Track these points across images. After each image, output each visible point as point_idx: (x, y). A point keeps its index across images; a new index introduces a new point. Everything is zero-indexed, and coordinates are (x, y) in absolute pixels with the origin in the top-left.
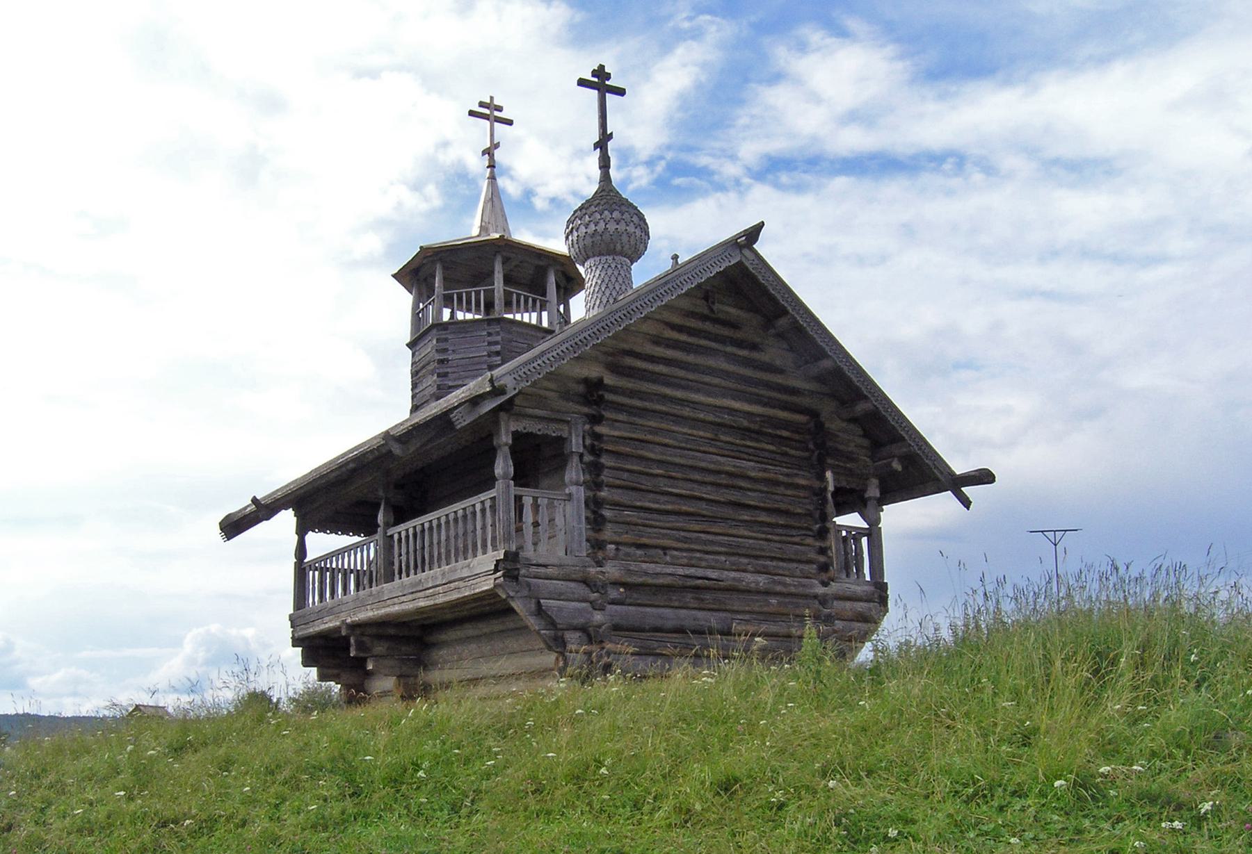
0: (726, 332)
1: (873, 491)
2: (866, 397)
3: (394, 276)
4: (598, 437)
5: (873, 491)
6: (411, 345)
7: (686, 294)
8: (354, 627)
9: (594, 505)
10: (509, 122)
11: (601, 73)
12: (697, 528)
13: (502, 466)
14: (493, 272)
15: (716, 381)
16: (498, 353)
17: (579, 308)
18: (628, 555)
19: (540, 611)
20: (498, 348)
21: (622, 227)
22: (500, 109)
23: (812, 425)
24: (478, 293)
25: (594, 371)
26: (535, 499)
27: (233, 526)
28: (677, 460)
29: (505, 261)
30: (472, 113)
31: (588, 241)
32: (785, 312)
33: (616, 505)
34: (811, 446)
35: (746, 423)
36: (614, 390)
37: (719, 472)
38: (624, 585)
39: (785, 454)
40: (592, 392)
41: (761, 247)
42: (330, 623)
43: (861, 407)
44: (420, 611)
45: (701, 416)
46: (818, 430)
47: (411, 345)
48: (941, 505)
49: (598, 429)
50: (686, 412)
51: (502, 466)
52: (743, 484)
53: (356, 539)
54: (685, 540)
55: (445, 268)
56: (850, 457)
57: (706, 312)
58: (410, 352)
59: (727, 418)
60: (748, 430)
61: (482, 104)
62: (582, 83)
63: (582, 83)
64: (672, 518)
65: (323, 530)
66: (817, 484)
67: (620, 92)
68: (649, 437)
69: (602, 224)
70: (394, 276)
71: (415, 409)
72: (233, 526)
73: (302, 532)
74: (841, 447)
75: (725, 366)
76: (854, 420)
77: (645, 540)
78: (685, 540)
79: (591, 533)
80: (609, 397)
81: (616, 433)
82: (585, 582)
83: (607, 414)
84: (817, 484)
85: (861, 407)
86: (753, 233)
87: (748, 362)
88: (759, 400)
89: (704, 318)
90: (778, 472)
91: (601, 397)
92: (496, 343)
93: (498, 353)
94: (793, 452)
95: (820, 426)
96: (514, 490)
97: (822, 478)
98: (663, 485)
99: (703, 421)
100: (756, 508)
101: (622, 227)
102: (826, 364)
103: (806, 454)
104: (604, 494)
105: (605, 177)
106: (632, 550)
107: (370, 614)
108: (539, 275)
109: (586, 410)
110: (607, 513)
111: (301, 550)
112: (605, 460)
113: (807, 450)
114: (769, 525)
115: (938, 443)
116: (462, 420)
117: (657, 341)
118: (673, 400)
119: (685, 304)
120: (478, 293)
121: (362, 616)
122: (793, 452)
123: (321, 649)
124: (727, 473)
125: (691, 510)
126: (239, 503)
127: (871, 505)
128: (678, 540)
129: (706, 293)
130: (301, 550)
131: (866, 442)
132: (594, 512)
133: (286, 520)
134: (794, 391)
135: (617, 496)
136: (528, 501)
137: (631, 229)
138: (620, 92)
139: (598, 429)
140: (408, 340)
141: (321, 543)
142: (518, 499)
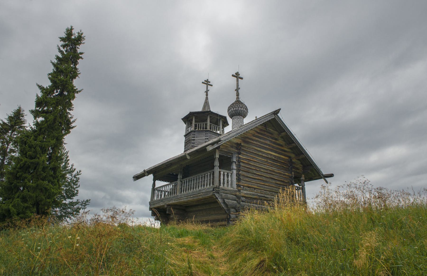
0: (270, 135)
1: (303, 178)
2: (303, 154)
3: (182, 119)
4: (239, 158)
5: (303, 178)
6: (185, 136)
7: (261, 125)
8: (168, 205)
9: (238, 175)
10: (212, 85)
11: (237, 74)
12: (263, 183)
13: (217, 163)
14: (207, 119)
15: (267, 147)
16: (208, 139)
17: (228, 129)
18: (246, 189)
19: (224, 202)
20: (208, 137)
21: (242, 109)
22: (210, 82)
23: (289, 160)
24: (203, 124)
25: (239, 141)
26: (224, 172)
27: (137, 177)
28: (258, 165)
29: (210, 117)
30: (203, 83)
31: (234, 112)
32: (284, 131)
33: (243, 176)
34: (289, 165)
35: (274, 158)
36: (243, 146)
37: (268, 170)
38: (245, 197)
39: (283, 167)
40: (238, 146)
41: (279, 115)
42: (161, 204)
43: (301, 157)
44: (184, 202)
45: (264, 155)
46: (291, 162)
47: (185, 136)
48: (321, 182)
49: (239, 156)
50: (260, 154)
51: (217, 163)
52: (273, 173)
53: (168, 183)
54: (260, 187)
55: (195, 118)
56: (298, 169)
57: (265, 130)
58: (184, 138)
59: (269, 156)
60: (274, 160)
61: (205, 81)
62: (233, 76)
63: (233, 76)
64: (256, 180)
65: (160, 180)
66: (290, 175)
67: (242, 78)
68: (252, 159)
69: (237, 108)
70: (182, 119)
71: (185, 151)
72: (137, 177)
73: (154, 180)
74: (295, 166)
75: (269, 143)
76: (299, 160)
77: (250, 186)
78: (260, 187)
79: (237, 183)
80: (242, 148)
81: (244, 157)
82: (236, 195)
83: (242, 152)
84: (290, 175)
85: (301, 157)
86: (276, 112)
87: (274, 143)
88: (276, 152)
89: (264, 131)
90: (281, 171)
91: (241, 148)
92: (193, 143)
93: (208, 139)
94: (285, 166)
95: (291, 160)
96: (219, 170)
97: (292, 174)
98: (255, 172)
99: (264, 156)
100: (276, 180)
101: (242, 109)
102: (294, 144)
103: (288, 167)
104: (241, 172)
105: (238, 98)
106: (247, 188)
107: (174, 202)
108: (219, 121)
109: (237, 151)
110: (241, 178)
111: (154, 184)
112: (242, 164)
113: (288, 166)
114: (279, 184)
115: (319, 166)
116: (210, 148)
117: (254, 135)
118: (257, 150)
119: (260, 127)
120: (203, 124)
121: (171, 202)
122: (285, 166)
123: (160, 212)
124: (270, 170)
125: (261, 179)
126: (140, 171)
127: (302, 182)
128: (258, 186)
129: (265, 125)
130: (154, 184)
131: (302, 166)
132: (238, 177)
133: (151, 177)
134: (285, 151)
135: (244, 173)
136: (222, 173)
137: (244, 110)
138: (242, 78)
139: (239, 156)
140: (184, 134)
141: (159, 184)
142: (220, 172)
